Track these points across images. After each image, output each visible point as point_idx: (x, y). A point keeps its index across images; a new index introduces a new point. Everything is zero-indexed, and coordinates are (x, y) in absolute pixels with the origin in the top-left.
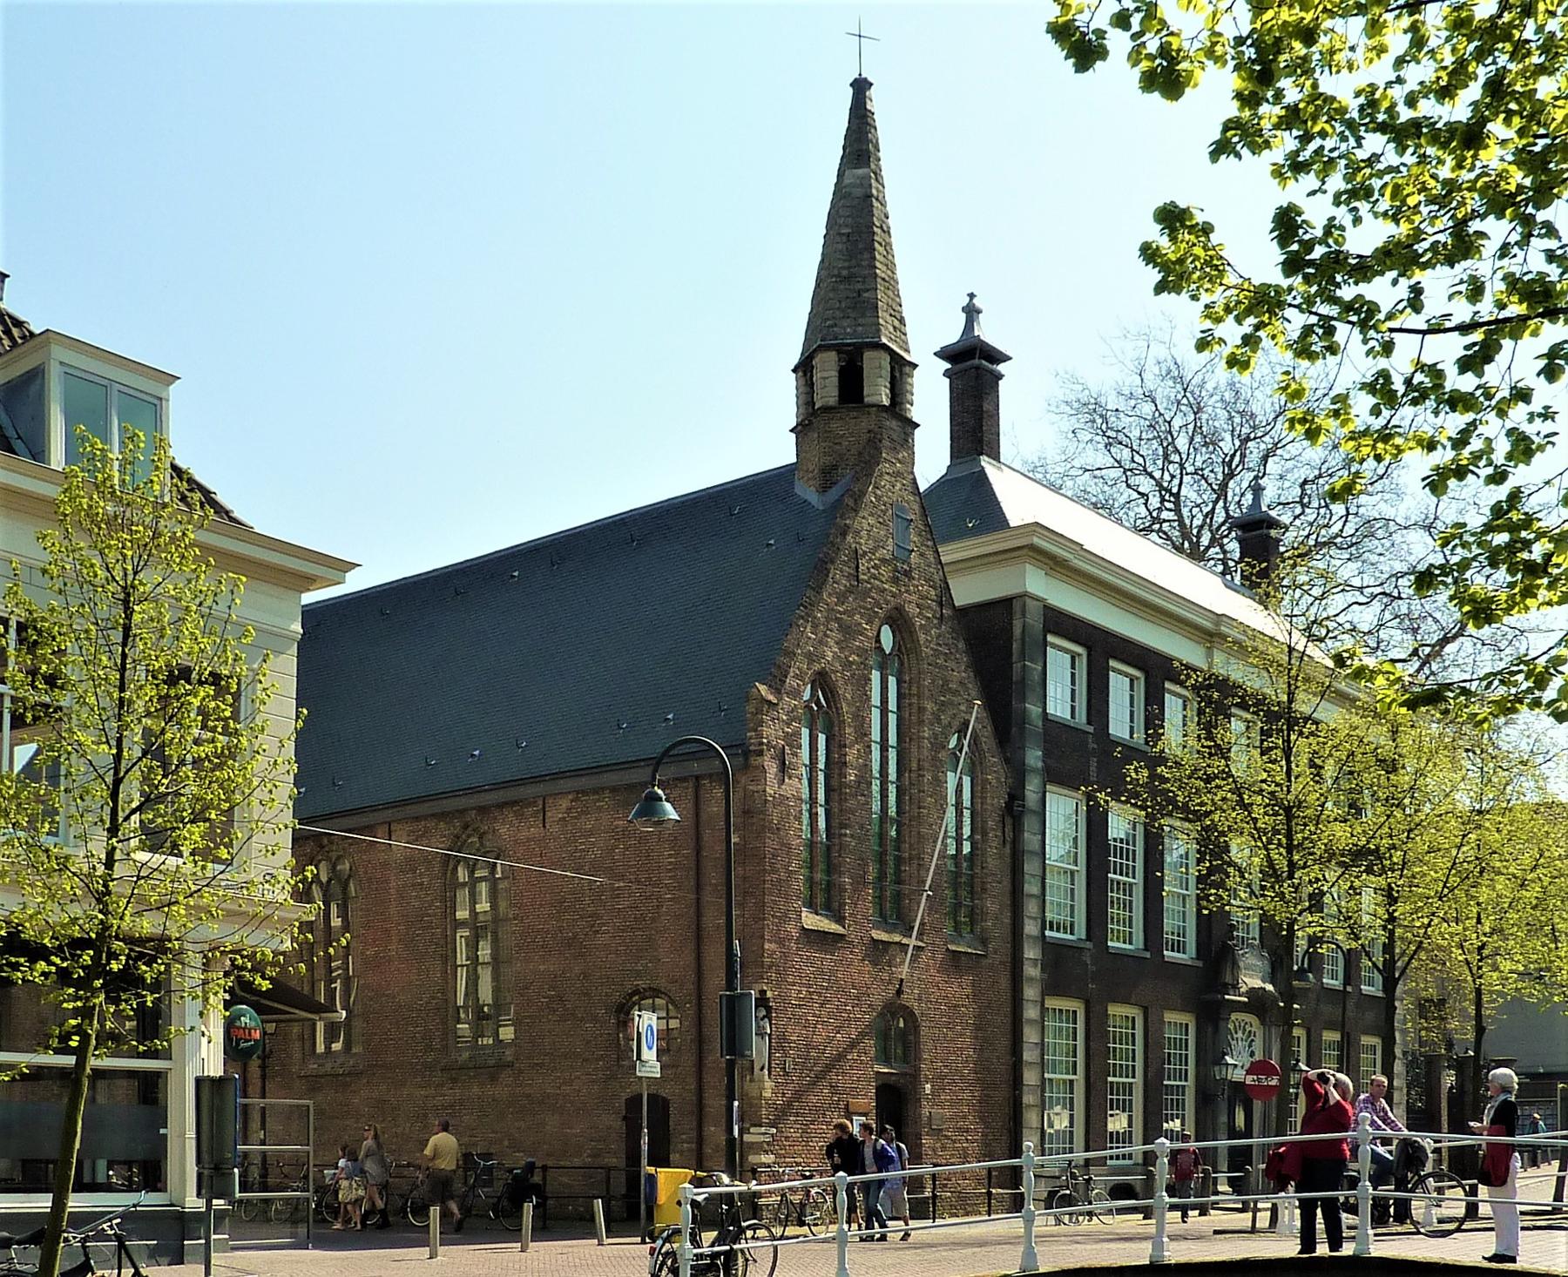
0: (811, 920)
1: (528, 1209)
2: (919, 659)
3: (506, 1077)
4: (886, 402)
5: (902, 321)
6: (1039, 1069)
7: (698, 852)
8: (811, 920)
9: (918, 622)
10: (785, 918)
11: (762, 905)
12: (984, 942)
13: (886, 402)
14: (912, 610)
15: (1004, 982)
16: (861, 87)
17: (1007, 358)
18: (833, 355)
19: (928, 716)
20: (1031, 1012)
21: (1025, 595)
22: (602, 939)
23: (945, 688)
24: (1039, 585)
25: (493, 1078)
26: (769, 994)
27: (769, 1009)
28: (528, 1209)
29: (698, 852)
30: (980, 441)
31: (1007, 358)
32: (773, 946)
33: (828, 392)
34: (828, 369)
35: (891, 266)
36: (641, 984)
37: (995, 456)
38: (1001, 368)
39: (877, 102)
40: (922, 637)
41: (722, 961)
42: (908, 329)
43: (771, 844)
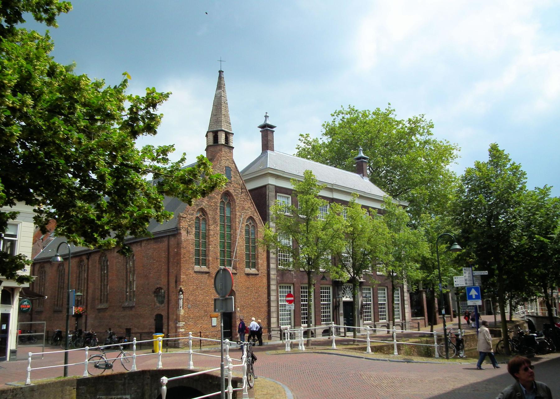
0: (248, 270)
1: (486, 273)
2: (235, 202)
3: (134, 309)
4: (223, 143)
5: (230, 124)
6: (276, 291)
7: (169, 253)
8: (197, 268)
9: (233, 194)
10: (188, 269)
11: (180, 266)
12: (258, 270)
13: (223, 143)
14: (231, 191)
15: (265, 280)
16: (221, 72)
17: (275, 127)
18: (211, 133)
19: (237, 216)
20: (273, 287)
21: (269, 184)
22: (151, 275)
23: (243, 208)
24: (272, 181)
25: (131, 309)
26: (183, 289)
27: (183, 292)
28: (486, 273)
29: (169, 253)
30: (268, 147)
31: (275, 127)
32: (184, 276)
33: (211, 143)
34: (211, 136)
35: (227, 111)
36: (158, 286)
37: (273, 150)
38: (274, 129)
39: (225, 75)
40: (235, 197)
41: (174, 280)
42: (232, 126)
43: (183, 251)
